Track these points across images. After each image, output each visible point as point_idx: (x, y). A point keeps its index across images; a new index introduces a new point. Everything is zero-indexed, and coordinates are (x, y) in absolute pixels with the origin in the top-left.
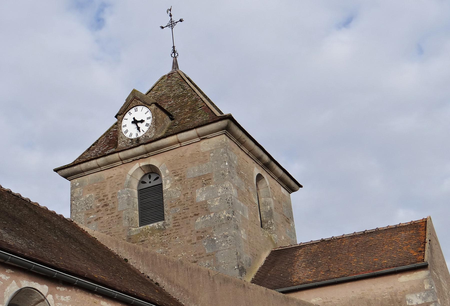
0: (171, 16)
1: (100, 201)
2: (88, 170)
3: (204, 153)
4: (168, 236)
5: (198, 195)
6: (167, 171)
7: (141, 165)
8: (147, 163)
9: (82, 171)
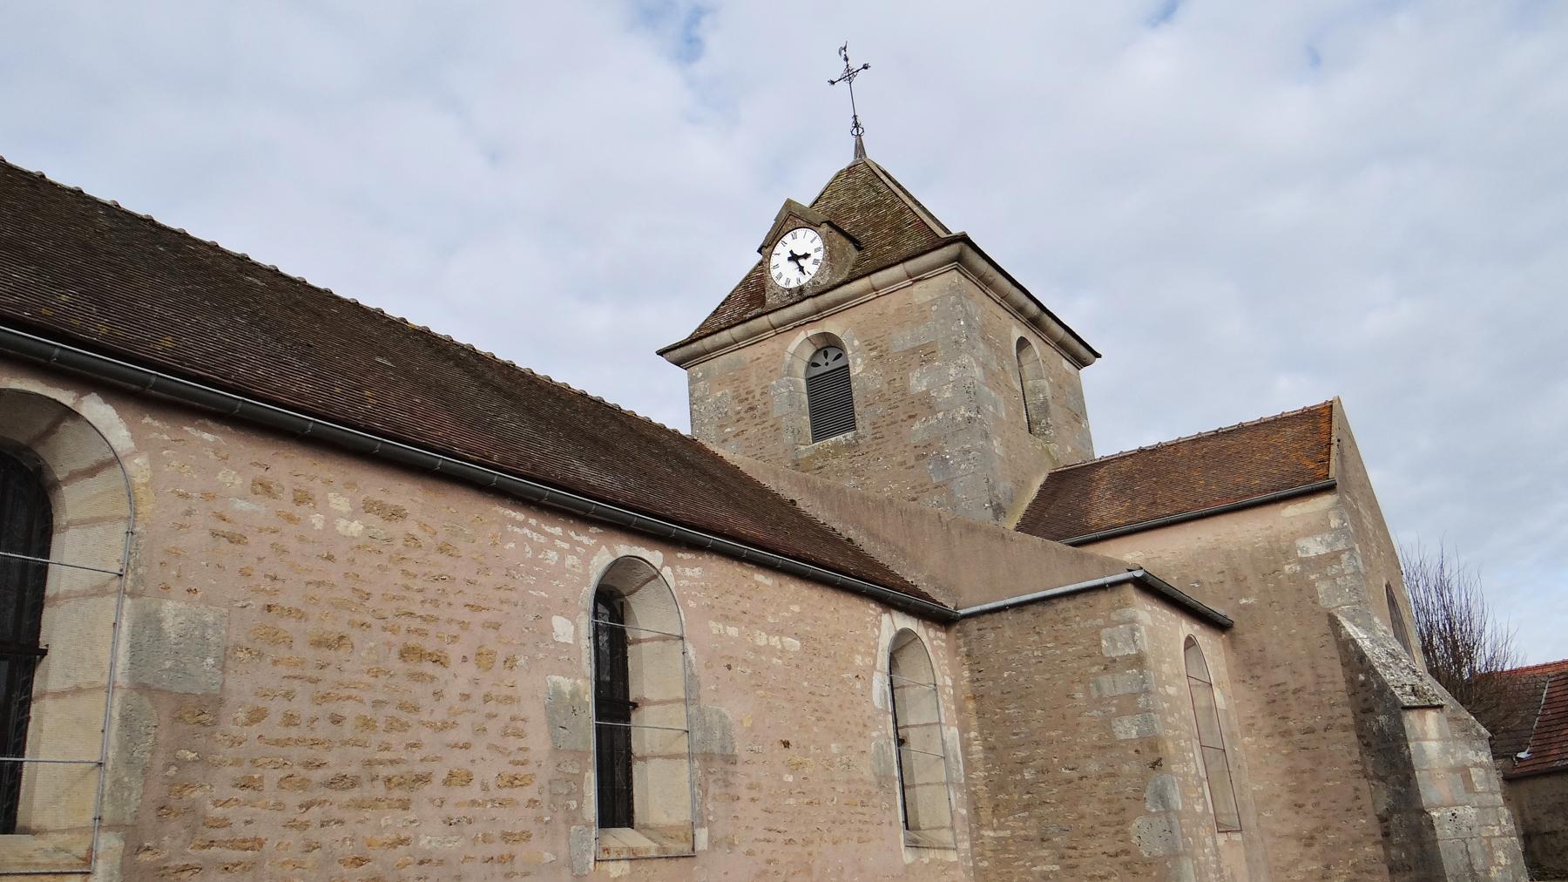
1: (741, 401)
2: (715, 349)
3: (920, 307)
5: (913, 382)
6: (856, 343)
8: (820, 331)
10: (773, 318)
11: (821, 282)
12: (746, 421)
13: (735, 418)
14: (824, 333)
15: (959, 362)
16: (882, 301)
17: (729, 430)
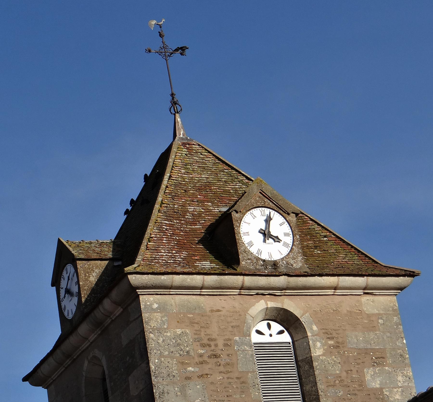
0: (161, 35)
1: (203, 346)
3: (369, 316)
5: (368, 377)
6: (315, 328)
8: (279, 305)
9: (171, 287)
10: (238, 280)
11: (294, 265)
12: (210, 366)
13: (197, 360)
15: (405, 373)
16: (337, 299)
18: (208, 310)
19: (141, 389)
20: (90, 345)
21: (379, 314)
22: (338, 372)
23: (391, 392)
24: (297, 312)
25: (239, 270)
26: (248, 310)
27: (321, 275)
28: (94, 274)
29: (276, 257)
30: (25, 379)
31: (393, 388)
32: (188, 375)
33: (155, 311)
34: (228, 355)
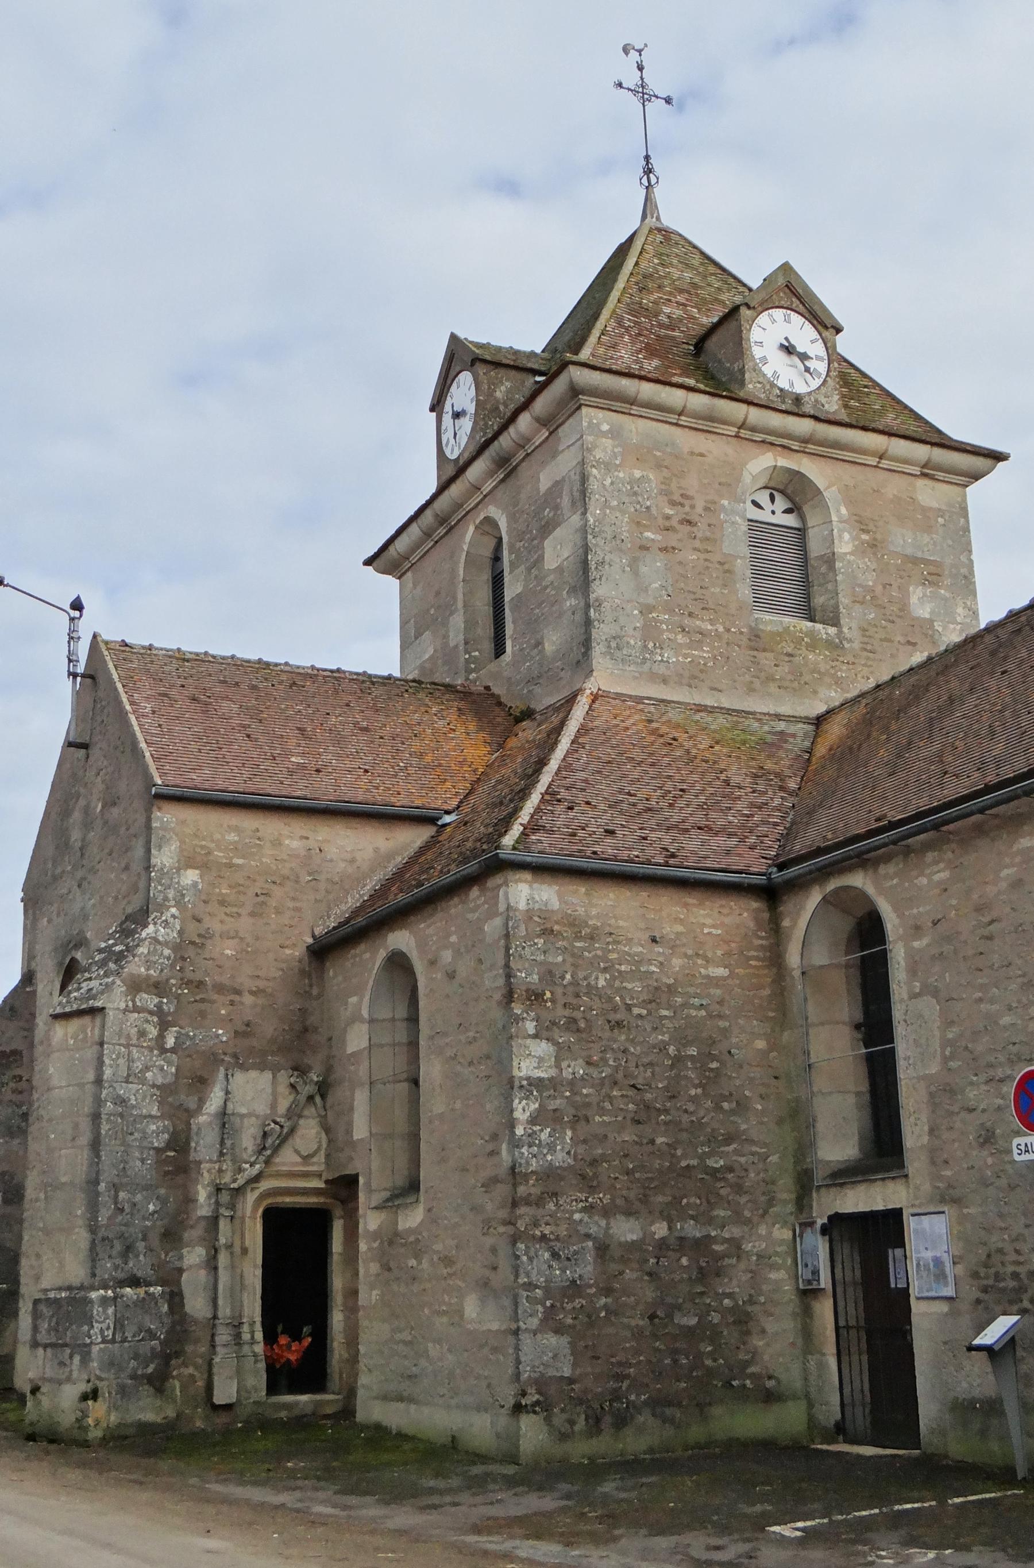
0: (641, 68)
1: (673, 503)
2: (648, 405)
3: (925, 510)
4: (851, 667)
5: (914, 600)
6: (844, 511)
7: (779, 464)
8: (795, 467)
9: (633, 402)
11: (827, 406)
12: (680, 536)
13: (661, 521)
14: (798, 472)
16: (882, 475)
17: (942, 592)
18: (686, 450)
19: (566, 556)
20: (482, 500)
21: (939, 510)
22: (871, 583)
23: (945, 628)
24: (820, 483)
25: (742, 394)
26: (746, 464)
27: (865, 429)
28: (503, 388)
29: (800, 388)
30: (368, 562)
31: (948, 622)
32: (644, 543)
33: (604, 434)
34: (709, 525)
